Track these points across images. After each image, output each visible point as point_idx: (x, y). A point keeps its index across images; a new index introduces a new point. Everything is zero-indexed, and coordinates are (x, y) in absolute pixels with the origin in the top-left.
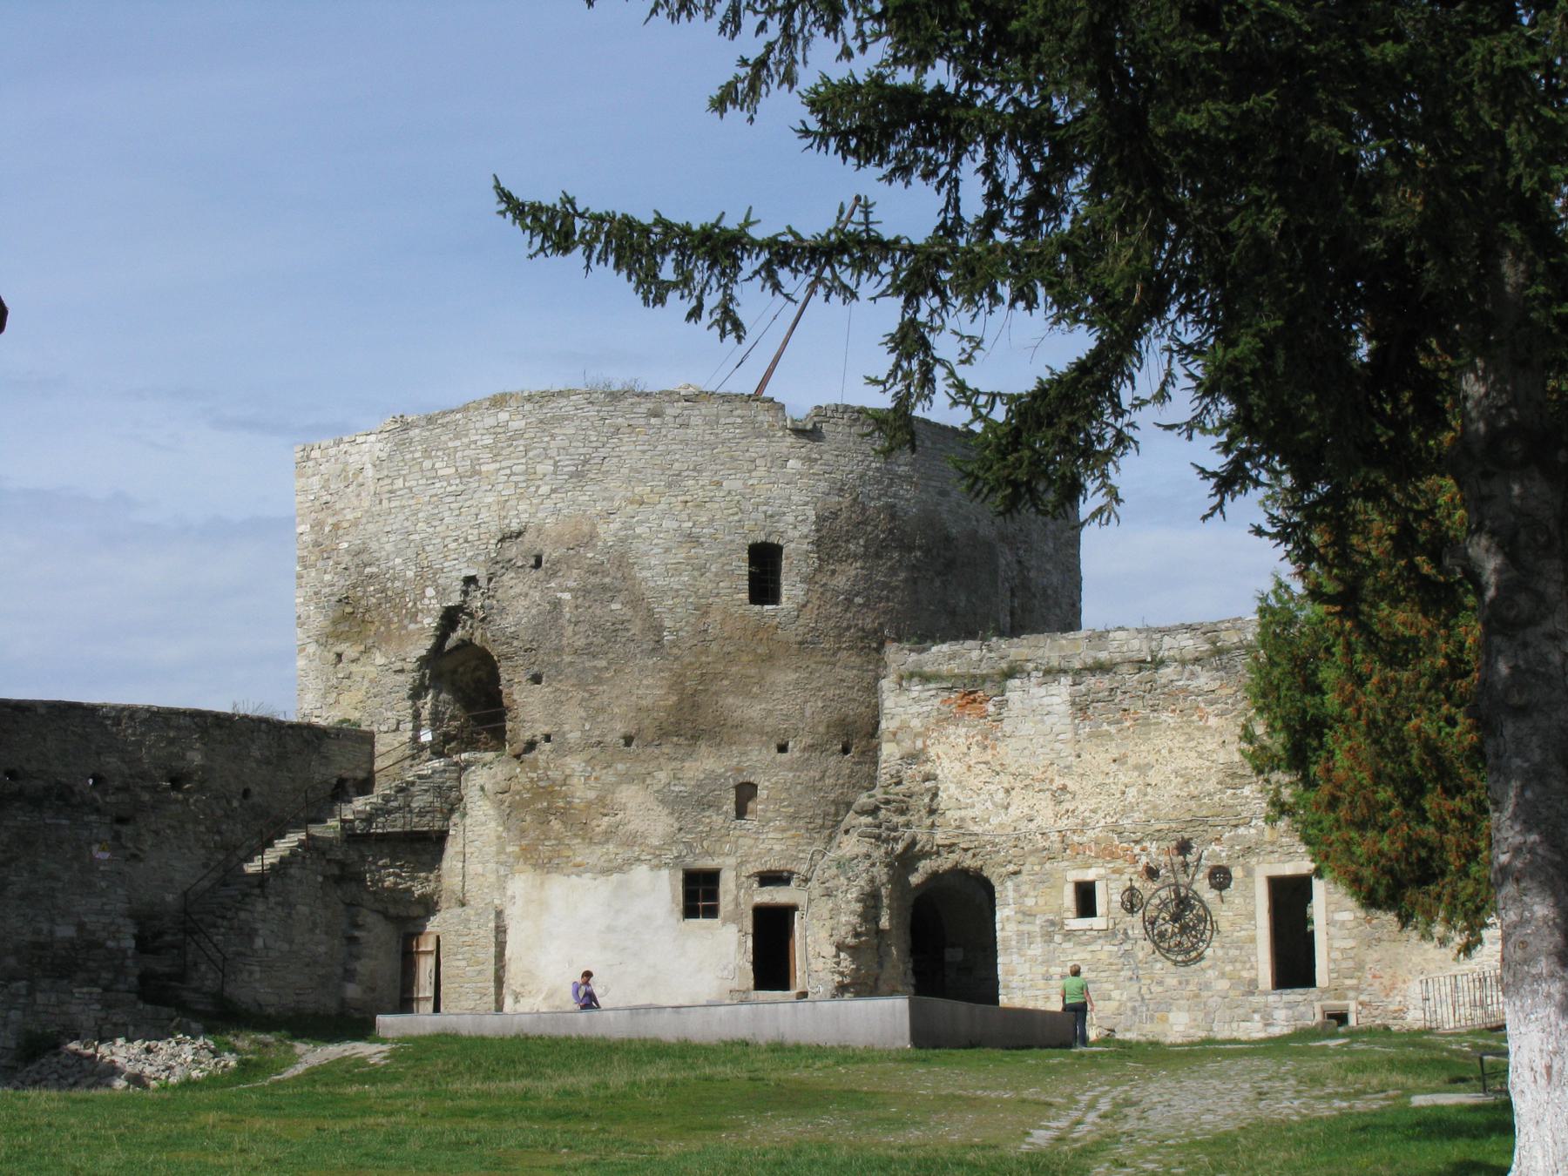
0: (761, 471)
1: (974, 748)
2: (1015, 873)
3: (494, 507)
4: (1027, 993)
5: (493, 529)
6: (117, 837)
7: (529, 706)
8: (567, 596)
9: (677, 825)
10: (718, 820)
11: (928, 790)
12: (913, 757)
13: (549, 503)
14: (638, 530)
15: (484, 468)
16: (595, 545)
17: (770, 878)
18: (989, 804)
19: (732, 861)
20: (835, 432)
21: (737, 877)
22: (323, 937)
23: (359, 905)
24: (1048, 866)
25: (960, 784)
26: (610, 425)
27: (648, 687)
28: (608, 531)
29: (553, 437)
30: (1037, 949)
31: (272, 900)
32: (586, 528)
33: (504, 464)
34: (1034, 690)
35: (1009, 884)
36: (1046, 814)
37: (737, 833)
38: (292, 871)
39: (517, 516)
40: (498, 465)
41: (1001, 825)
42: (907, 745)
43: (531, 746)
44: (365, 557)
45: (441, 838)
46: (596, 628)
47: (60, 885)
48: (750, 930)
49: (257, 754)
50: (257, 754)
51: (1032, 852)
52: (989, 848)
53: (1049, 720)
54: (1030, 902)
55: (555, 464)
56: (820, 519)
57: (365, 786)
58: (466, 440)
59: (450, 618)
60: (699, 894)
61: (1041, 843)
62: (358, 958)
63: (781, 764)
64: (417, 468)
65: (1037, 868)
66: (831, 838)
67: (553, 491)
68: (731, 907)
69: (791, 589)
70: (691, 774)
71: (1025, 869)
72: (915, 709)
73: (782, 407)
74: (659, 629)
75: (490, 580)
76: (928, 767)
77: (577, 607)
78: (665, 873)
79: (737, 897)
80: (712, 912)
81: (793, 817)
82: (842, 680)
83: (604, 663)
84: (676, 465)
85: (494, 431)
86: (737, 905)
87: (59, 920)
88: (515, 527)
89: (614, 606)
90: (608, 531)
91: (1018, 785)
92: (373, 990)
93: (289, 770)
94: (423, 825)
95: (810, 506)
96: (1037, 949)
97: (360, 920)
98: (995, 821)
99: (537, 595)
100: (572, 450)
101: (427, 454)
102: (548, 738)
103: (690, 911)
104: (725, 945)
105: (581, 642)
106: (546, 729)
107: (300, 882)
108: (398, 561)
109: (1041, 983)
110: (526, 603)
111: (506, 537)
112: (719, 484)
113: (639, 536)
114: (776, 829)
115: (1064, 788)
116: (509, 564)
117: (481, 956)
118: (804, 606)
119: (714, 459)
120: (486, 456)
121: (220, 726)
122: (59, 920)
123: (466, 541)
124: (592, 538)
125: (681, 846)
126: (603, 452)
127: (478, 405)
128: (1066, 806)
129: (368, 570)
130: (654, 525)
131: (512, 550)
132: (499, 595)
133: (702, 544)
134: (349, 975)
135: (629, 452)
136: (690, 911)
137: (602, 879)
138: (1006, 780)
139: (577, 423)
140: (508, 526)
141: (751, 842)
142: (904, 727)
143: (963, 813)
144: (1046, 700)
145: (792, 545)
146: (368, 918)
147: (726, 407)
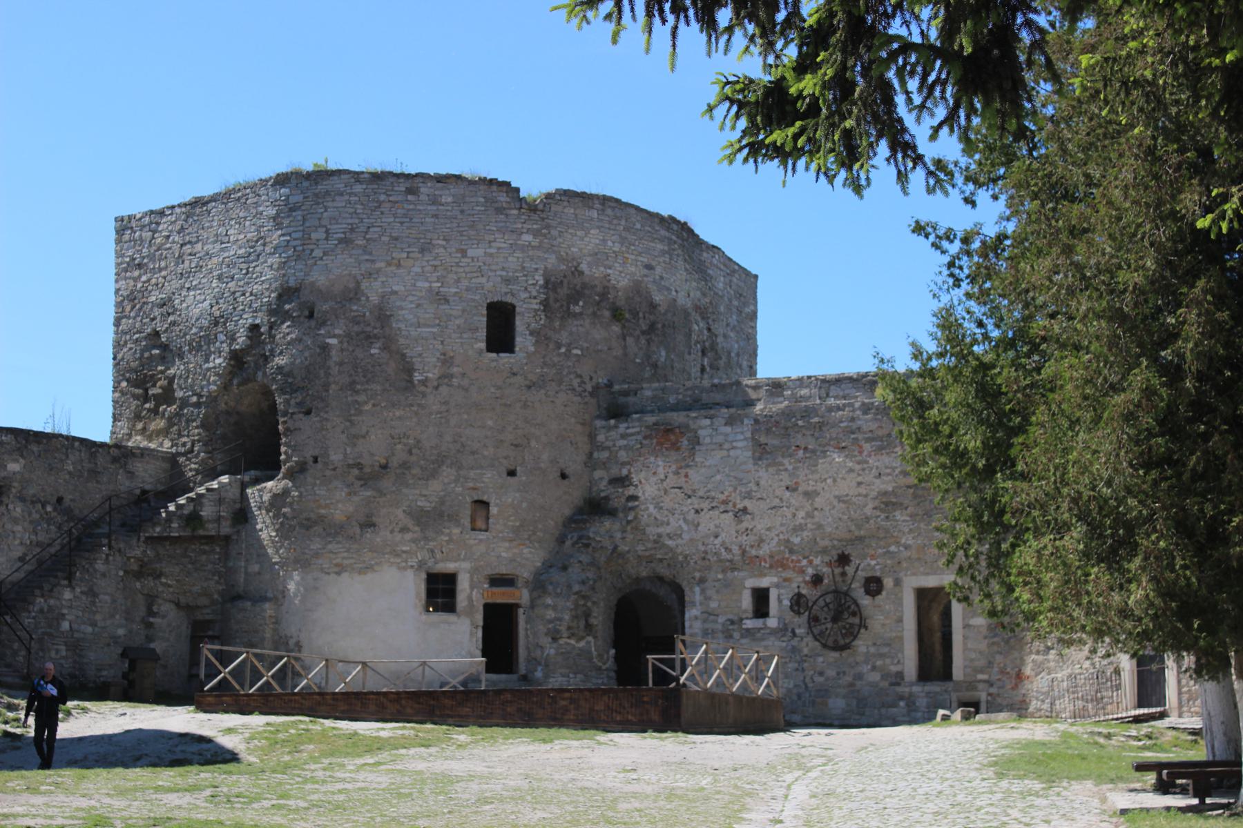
8: (333, 341)
17: (498, 581)
22: (123, 622)
42: (615, 471)
48: (481, 623)
49: (71, 468)
54: (713, 605)
55: (327, 232)
60: (440, 592)
69: (523, 340)
89: (373, 351)
91: (706, 505)
93: (98, 482)
106: (316, 453)
107: (104, 575)
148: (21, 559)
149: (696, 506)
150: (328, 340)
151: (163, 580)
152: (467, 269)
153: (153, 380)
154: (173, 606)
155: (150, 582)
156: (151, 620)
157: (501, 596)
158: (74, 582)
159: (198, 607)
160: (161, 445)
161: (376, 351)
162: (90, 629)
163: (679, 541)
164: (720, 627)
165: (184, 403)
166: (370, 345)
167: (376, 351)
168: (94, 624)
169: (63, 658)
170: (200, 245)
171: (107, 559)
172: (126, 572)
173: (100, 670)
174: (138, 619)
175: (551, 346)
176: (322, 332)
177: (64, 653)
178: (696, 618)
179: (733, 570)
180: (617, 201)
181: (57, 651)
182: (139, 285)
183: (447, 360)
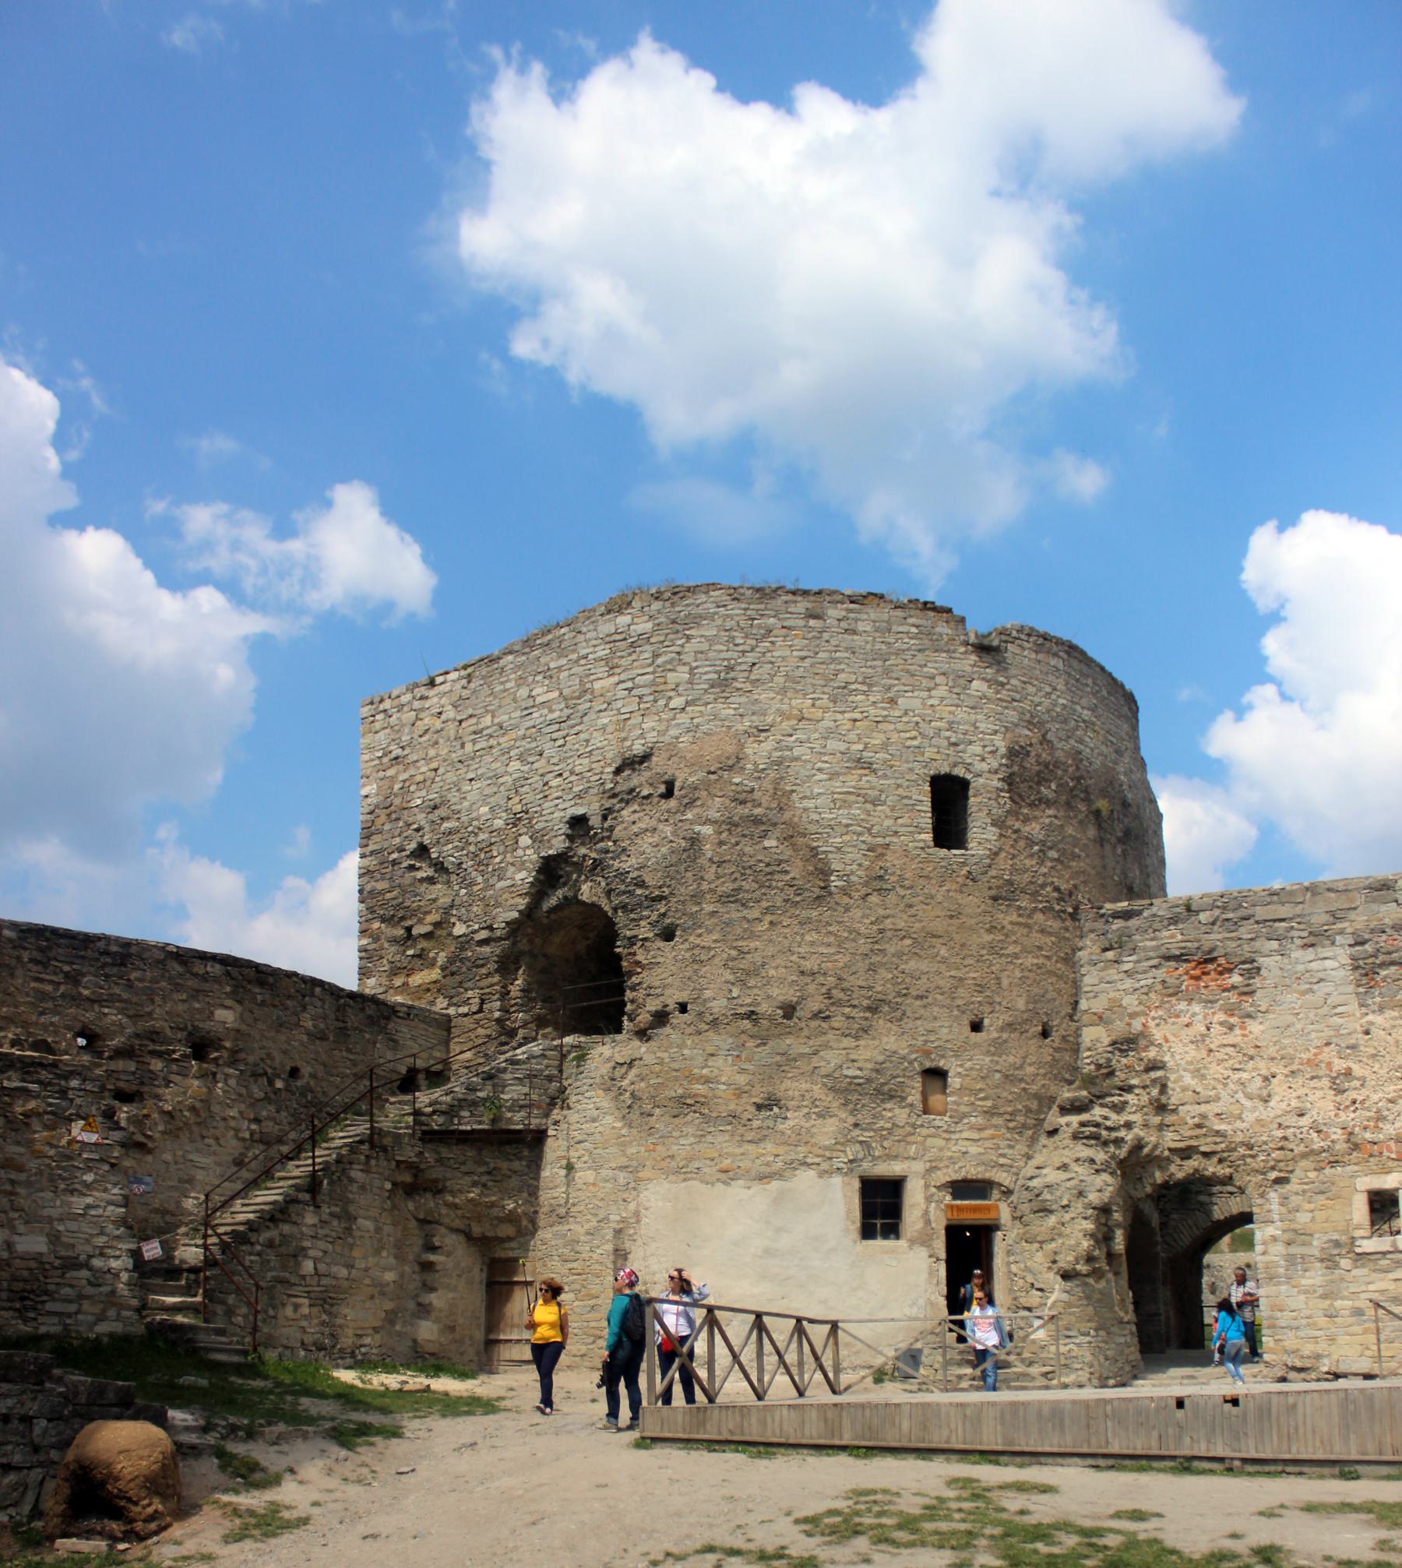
0: (941, 691)
1: (1216, 1029)
2: (1278, 1181)
3: (610, 729)
4: (1301, 1334)
5: (610, 755)
6: (109, 1115)
7: (659, 974)
8: (707, 830)
9: (851, 1120)
10: (901, 1115)
11: (1154, 1081)
12: (1126, 1044)
13: (683, 719)
14: (796, 752)
15: (597, 685)
16: (743, 769)
17: (963, 1188)
18: (1240, 1096)
19: (919, 1167)
20: (1019, 655)
21: (927, 1186)
22: (392, 1260)
23: (438, 1223)
24: (1328, 1171)
25: (1198, 1073)
26: (759, 627)
27: (812, 944)
28: (759, 752)
29: (688, 638)
30: (1315, 1277)
31: (325, 1209)
32: (731, 749)
33: (623, 677)
34: (1297, 954)
35: (1273, 1195)
36: (1322, 1104)
37: (924, 1131)
38: (353, 1174)
39: (642, 736)
40: (616, 679)
41: (1258, 1121)
42: (1119, 1028)
43: (661, 1018)
44: (442, 812)
45: (539, 1138)
46: (745, 870)
47: (23, 1176)
48: (943, 1255)
49: (309, 1024)
50: (309, 1024)
51: (1304, 1156)
52: (1242, 1151)
53: (1323, 988)
54: (1303, 1218)
55: (691, 672)
56: (1012, 753)
57: (437, 1077)
58: (574, 656)
59: (551, 871)
60: (881, 1207)
61: (1318, 1143)
62: (433, 1289)
63: (976, 1045)
64: (508, 700)
65: (1312, 1175)
66: (1033, 1140)
67: (688, 703)
68: (920, 1225)
69: (981, 833)
70: (868, 1054)
71: (1294, 1179)
72: (1129, 984)
73: (962, 620)
74: (824, 873)
75: (605, 818)
76: (1152, 1053)
77: (721, 843)
78: (837, 1180)
79: (926, 1213)
80: (892, 1230)
81: (990, 1113)
82: (1040, 948)
83: (756, 914)
84: (842, 676)
85: (609, 640)
86: (928, 1222)
87: (22, 1228)
88: (638, 749)
89: (767, 843)
90: (759, 752)
91: (1279, 1069)
92: (452, 1329)
93: (349, 1050)
94: (517, 1121)
95: (999, 737)
96: (1315, 1277)
97: (436, 1241)
98: (1250, 1117)
99: (668, 830)
100: (711, 655)
101: (521, 681)
102: (683, 1008)
103: (868, 1232)
104: (913, 1269)
105: (728, 887)
106: (683, 996)
107: (363, 1188)
108: (484, 810)
109: (1322, 1321)
110: (655, 839)
111: (631, 763)
112: (893, 701)
113: (797, 759)
114: (972, 1128)
115: (1348, 1073)
116: (631, 796)
117: (595, 1289)
118: (996, 854)
119: (887, 672)
120: (601, 670)
121: (262, 983)
122: (22, 1228)
123: (572, 773)
124: (739, 759)
125: (858, 1147)
126: (750, 658)
127: (588, 614)
128: (1352, 1095)
129: (446, 825)
130: (817, 746)
131: (637, 779)
132: (618, 832)
133: (875, 771)
134: (424, 1310)
135: (784, 658)
136: (868, 1232)
137: (757, 1187)
138: (1263, 1067)
139: (719, 622)
140: (630, 748)
141: (941, 1143)
142: (1115, 1006)
143: (1203, 1108)
144: (1314, 965)
145: (981, 780)
146: (445, 1238)
147: (899, 613)
148: (239, 1163)
149: (1264, 1072)
150: (697, 828)
151: (450, 1198)
152: (900, 726)
153: (418, 913)
154: (461, 1238)
155: (428, 1202)
156: (432, 1257)
157: (971, 1210)
158: (319, 1198)
159: (497, 1238)
160: (432, 1003)
161: (774, 843)
162: (343, 1272)
163: (1239, 1124)
164: (1317, 1253)
165: (465, 942)
166: (764, 836)
167: (774, 843)
168: (350, 1266)
169: (305, 1317)
170: (489, 718)
171: (367, 1163)
172: (394, 1184)
173: (361, 1336)
174: (411, 1257)
175: (1022, 844)
176: (689, 816)
177: (306, 1310)
178: (1274, 1239)
179: (1333, 1163)
180: (1083, 653)
181: (296, 1307)
182: (397, 787)
183: (878, 851)
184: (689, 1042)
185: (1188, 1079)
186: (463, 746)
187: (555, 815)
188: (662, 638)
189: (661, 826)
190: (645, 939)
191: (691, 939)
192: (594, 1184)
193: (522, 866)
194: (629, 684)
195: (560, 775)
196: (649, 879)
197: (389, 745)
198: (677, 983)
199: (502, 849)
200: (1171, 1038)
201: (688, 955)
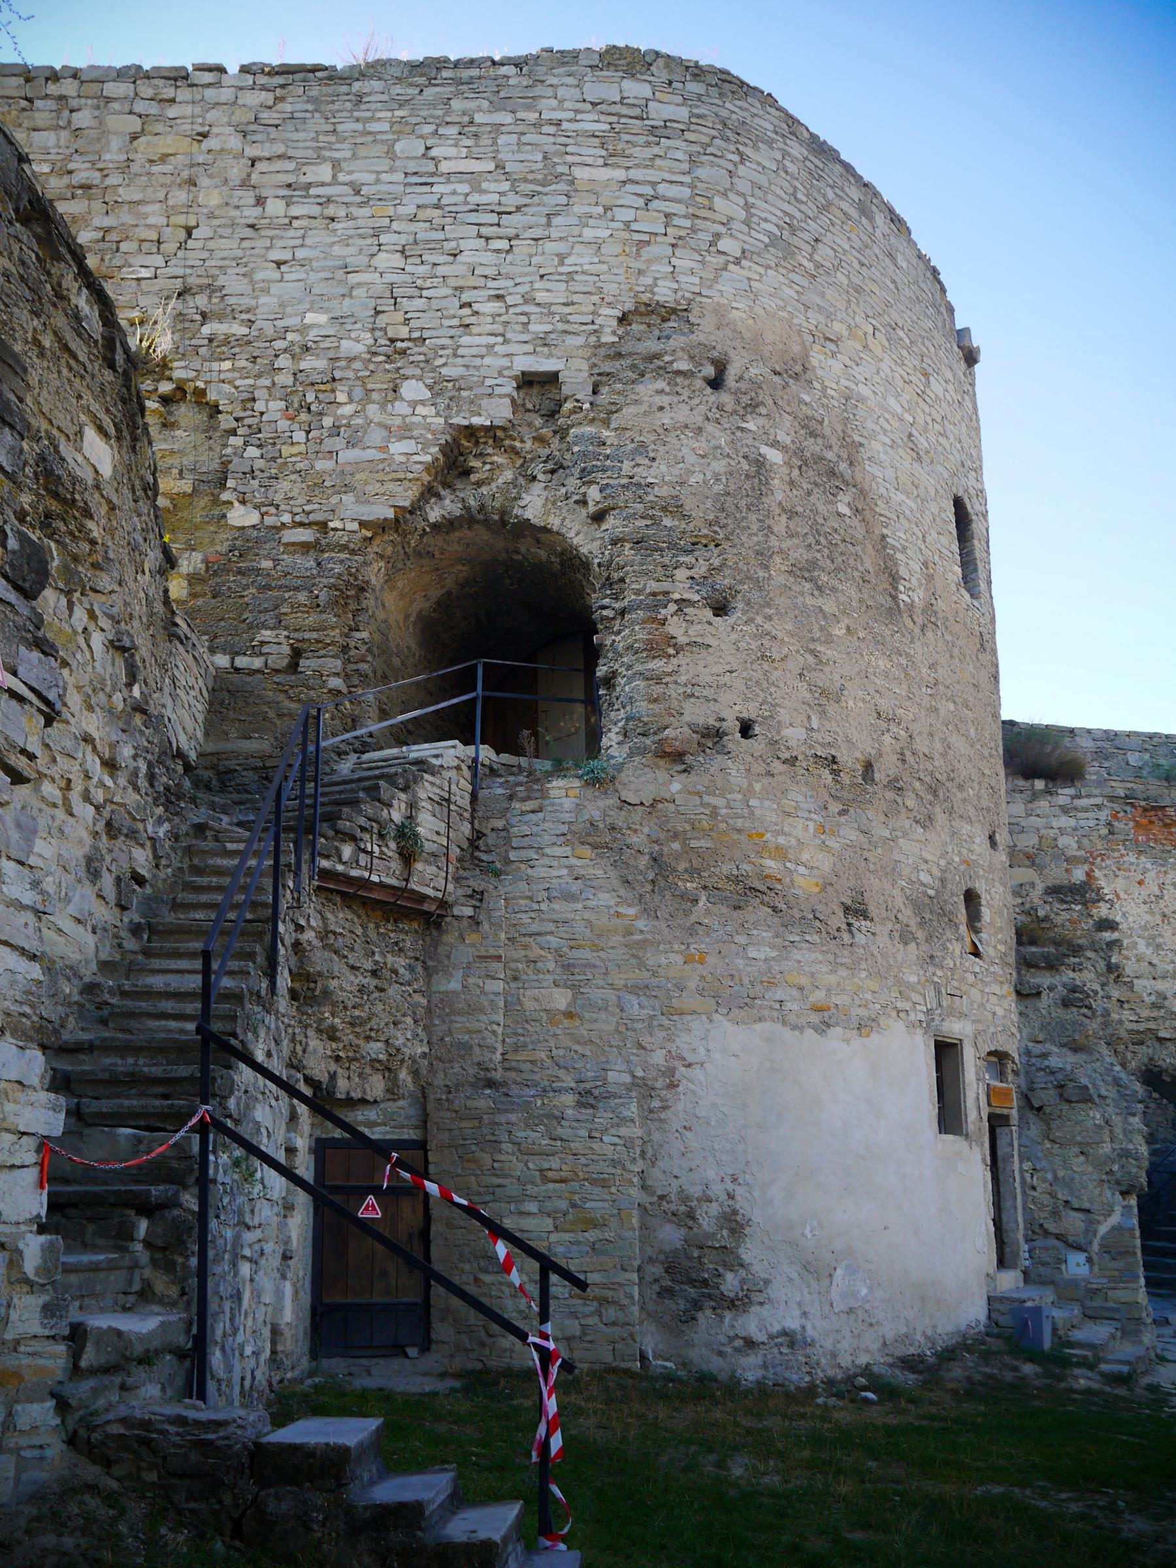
40: (620, 174)
58: (532, 116)
59: (456, 459)
72: (1064, 821)
76: (1102, 910)
106: (750, 711)
140: (651, 289)
150: (764, 450)
184: (758, 787)
185: (1142, 947)
186: (260, 201)
187: (491, 364)
188: (707, 140)
189: (710, 428)
190: (681, 602)
191: (759, 620)
192: (570, 1015)
193: (405, 432)
194: (648, 190)
195: (499, 297)
196: (689, 504)
197: (69, 158)
198: (739, 685)
199: (358, 393)
200: (1122, 895)
201: (754, 645)
